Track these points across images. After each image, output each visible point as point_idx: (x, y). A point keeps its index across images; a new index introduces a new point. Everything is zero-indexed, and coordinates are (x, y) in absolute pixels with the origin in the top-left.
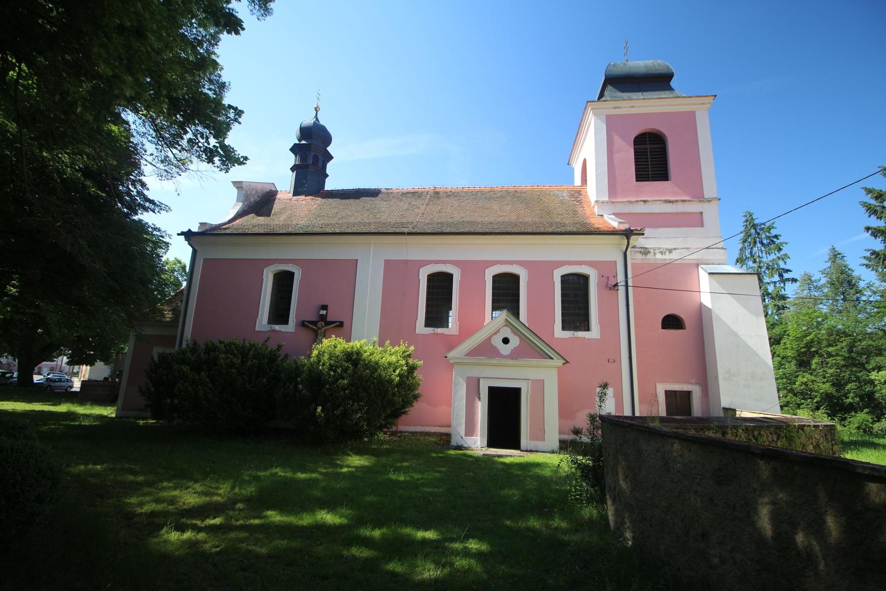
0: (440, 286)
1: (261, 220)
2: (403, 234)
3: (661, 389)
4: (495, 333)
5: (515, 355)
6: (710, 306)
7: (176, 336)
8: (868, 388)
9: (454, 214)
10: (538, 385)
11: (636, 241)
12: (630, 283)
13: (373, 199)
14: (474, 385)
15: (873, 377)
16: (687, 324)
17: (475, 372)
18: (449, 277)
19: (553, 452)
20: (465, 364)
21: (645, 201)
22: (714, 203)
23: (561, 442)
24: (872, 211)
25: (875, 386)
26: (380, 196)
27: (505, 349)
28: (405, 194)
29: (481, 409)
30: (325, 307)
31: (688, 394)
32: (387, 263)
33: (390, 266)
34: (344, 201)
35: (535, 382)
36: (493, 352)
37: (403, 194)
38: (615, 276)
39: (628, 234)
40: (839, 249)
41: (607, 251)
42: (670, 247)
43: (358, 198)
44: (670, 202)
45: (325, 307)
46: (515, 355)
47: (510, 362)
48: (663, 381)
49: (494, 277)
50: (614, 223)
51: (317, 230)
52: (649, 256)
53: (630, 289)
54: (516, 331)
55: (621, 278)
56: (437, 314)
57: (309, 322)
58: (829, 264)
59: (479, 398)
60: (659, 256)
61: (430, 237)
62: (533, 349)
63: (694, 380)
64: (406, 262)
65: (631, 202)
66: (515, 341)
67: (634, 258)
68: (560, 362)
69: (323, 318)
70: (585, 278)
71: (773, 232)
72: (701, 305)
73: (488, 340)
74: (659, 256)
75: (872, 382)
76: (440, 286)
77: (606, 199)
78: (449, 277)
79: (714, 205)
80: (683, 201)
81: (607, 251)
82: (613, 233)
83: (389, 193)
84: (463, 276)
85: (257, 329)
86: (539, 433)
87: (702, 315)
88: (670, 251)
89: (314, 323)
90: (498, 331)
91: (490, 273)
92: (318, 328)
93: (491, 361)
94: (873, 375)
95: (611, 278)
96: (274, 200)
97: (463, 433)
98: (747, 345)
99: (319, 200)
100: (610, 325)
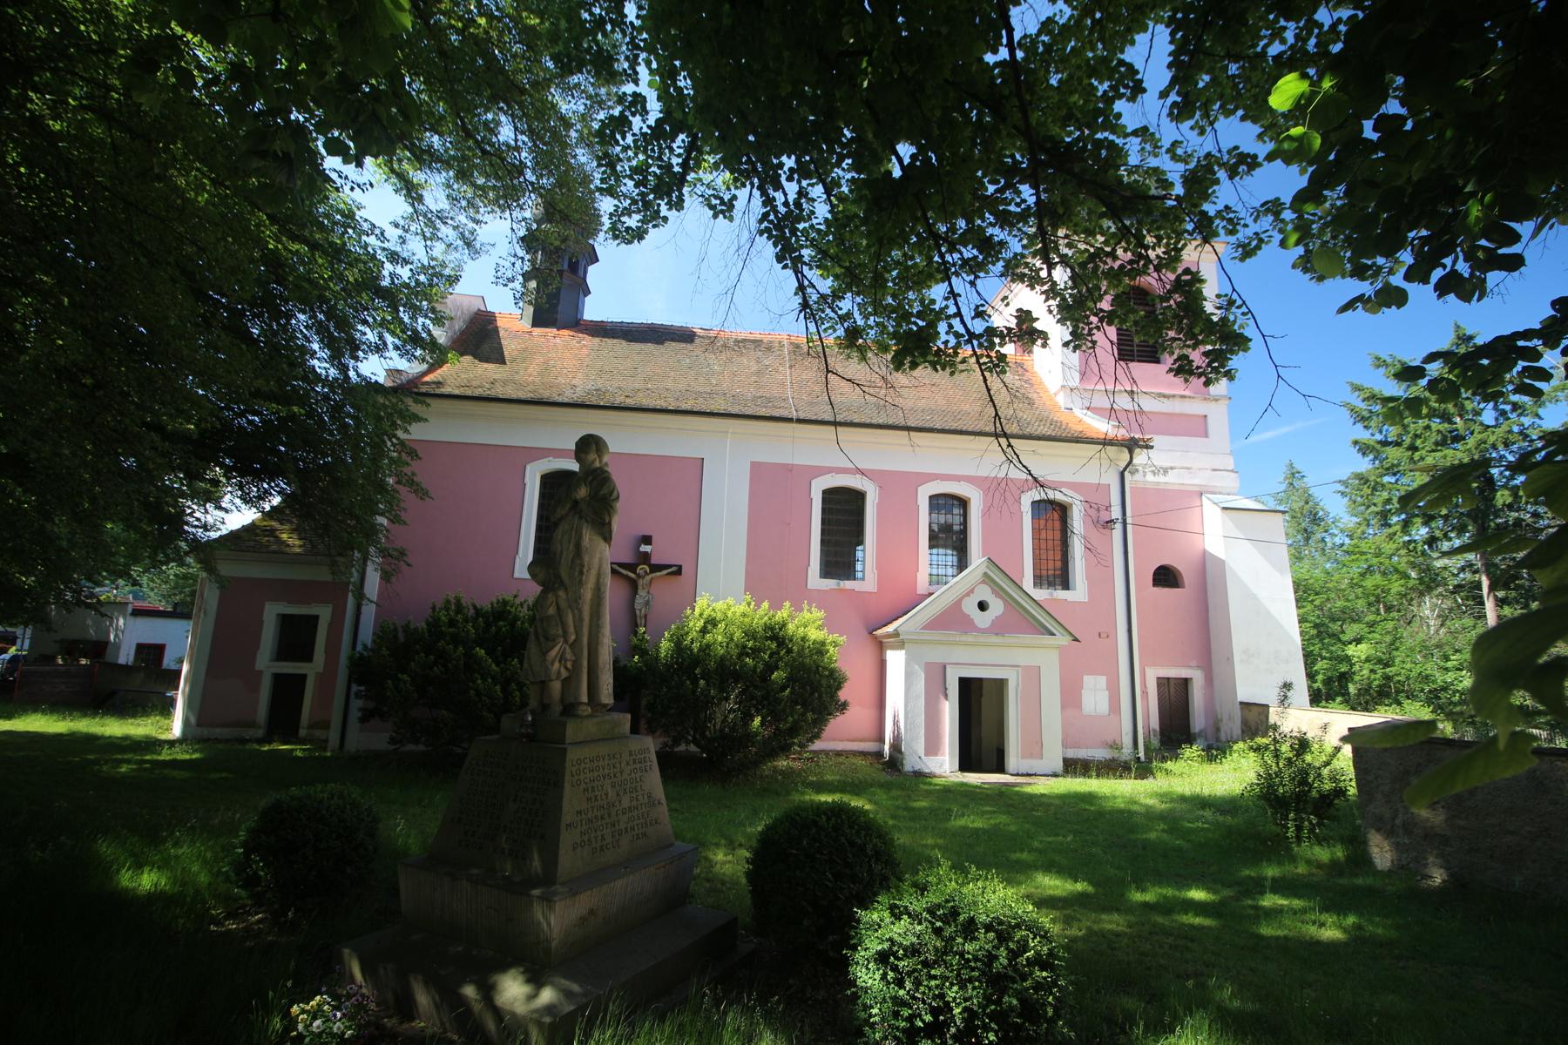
0: (844, 512)
1: (489, 370)
2: (789, 420)
3: (1152, 675)
4: (968, 595)
5: (998, 628)
6: (1222, 556)
8: (1344, 668)
10: (1033, 674)
11: (1140, 457)
12: (1129, 520)
13: (689, 346)
14: (936, 674)
15: (1350, 653)
17: (938, 655)
18: (857, 497)
19: (1055, 775)
20: (923, 642)
24: (1363, 419)
25: (1352, 665)
26: (697, 341)
27: (983, 620)
28: (741, 343)
29: (949, 712)
30: (647, 540)
31: (1185, 683)
32: (755, 466)
33: (761, 474)
35: (1027, 668)
36: (966, 625)
37: (737, 342)
39: (1131, 445)
40: (1298, 467)
41: (1095, 470)
42: (1165, 465)
44: (1165, 396)
45: (647, 540)
46: (998, 628)
47: (994, 639)
48: (1154, 665)
50: (1102, 426)
51: (619, 400)
52: (1138, 477)
53: (1129, 528)
54: (998, 591)
55: (1116, 513)
56: (839, 562)
58: (1283, 487)
59: (946, 696)
60: (1150, 478)
62: (1024, 621)
63: (1193, 663)
64: (789, 469)
66: (997, 607)
68: (1064, 640)
69: (645, 557)
71: (1364, 465)
72: (1205, 551)
73: (958, 603)
74: (1150, 478)
75: (1348, 659)
76: (844, 512)
78: (857, 497)
79: (1223, 404)
80: (1183, 397)
81: (1095, 470)
82: (1106, 442)
83: (713, 342)
86: (1035, 747)
87: (1208, 567)
88: (1166, 471)
89: (631, 567)
90: (972, 591)
91: (819, 486)
92: (639, 576)
93: (965, 638)
94: (1351, 650)
96: (496, 330)
97: (921, 752)
99: (587, 341)
100: (1101, 583)
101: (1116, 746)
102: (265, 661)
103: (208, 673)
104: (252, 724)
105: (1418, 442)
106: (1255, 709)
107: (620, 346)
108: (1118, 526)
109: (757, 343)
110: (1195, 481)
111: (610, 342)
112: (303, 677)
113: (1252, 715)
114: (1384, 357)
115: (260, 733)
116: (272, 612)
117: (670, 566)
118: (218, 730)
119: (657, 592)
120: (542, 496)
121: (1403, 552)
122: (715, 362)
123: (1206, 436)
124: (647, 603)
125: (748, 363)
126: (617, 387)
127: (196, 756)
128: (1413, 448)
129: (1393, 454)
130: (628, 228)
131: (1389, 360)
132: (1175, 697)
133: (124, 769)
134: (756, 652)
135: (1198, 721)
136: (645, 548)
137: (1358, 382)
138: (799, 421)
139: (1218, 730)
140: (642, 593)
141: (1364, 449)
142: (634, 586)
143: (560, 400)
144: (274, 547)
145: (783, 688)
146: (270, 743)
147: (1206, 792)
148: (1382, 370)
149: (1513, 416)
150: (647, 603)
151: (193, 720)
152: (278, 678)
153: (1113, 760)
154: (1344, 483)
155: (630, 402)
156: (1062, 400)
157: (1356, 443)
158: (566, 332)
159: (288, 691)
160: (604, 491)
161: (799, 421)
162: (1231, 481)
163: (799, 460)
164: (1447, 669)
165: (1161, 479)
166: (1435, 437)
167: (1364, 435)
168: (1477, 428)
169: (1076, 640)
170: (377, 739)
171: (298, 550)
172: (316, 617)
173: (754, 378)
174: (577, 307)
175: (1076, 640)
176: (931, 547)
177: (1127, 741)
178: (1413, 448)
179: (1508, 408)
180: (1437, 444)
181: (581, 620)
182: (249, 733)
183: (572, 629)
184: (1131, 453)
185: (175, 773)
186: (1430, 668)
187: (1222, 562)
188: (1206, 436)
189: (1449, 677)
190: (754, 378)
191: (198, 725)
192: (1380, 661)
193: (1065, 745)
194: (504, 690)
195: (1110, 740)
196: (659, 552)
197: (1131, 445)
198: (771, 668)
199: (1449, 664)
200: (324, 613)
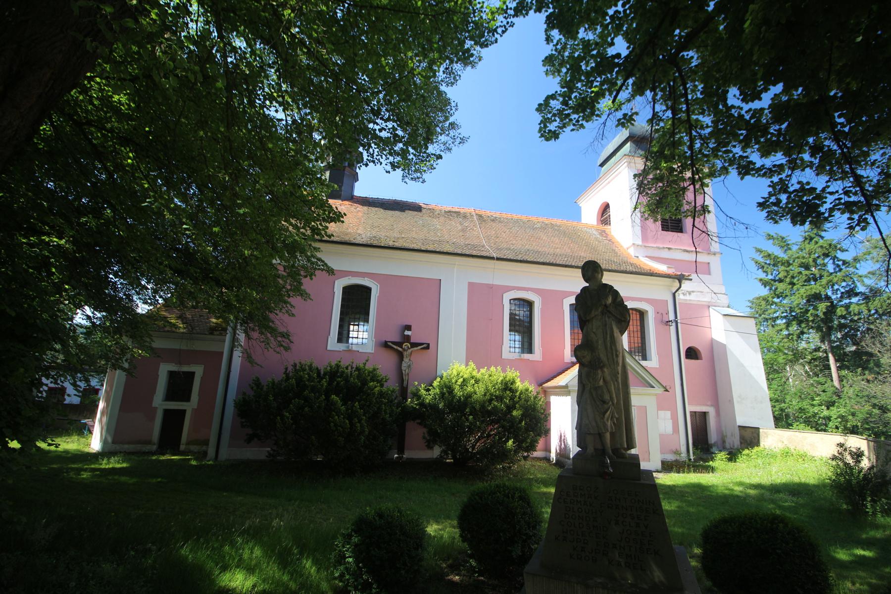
2: (493, 258)
7: (222, 353)
9: (480, 239)
16: (703, 355)
21: (669, 249)
22: (718, 256)
23: (663, 463)
26: (424, 211)
30: (409, 328)
31: (704, 415)
32: (471, 285)
34: (390, 213)
38: (667, 313)
41: (659, 291)
43: (404, 211)
44: (687, 251)
45: (409, 328)
49: (344, 288)
50: (662, 268)
55: (671, 317)
57: (393, 343)
61: (549, 267)
63: (709, 403)
64: (490, 287)
65: (659, 248)
67: (680, 297)
68: (659, 390)
70: (368, 290)
71: (764, 292)
77: (640, 243)
78: (366, 291)
79: (718, 257)
81: (659, 291)
84: (544, 304)
85: (329, 348)
87: (713, 345)
89: (400, 344)
91: (507, 297)
92: (404, 350)
95: (665, 315)
98: (750, 375)
101: (677, 452)
102: (159, 401)
103: (120, 410)
104: (149, 442)
105: (795, 281)
106: (748, 430)
107: (380, 211)
108: (674, 324)
109: (458, 213)
110: (706, 298)
111: (374, 209)
112: (184, 411)
113: (748, 434)
114: (772, 234)
115: (155, 448)
116: (164, 369)
117: (423, 344)
118: (126, 446)
119: (415, 361)
120: (343, 300)
121: (786, 340)
122: (437, 223)
123: (710, 274)
124: (409, 366)
125: (455, 224)
126: (386, 236)
127: (125, 465)
128: (793, 284)
129: (781, 287)
130: (550, 131)
131: (775, 236)
132: (700, 423)
133: (85, 475)
134: (500, 399)
135: (713, 437)
136: (407, 333)
137: (759, 247)
138: (498, 259)
139: (724, 442)
140: (406, 360)
141: (765, 283)
142: (401, 356)
143: (354, 241)
144: (167, 329)
145: (521, 421)
146: (163, 454)
147: (778, 481)
148: (771, 241)
149: (843, 267)
150: (409, 366)
151: (110, 440)
152: (167, 412)
153: (676, 461)
154: (752, 302)
155: (397, 244)
156: (632, 252)
157: (761, 280)
158: (347, 202)
159: (173, 420)
160: (619, 300)
161: (498, 259)
162: (724, 300)
163: (498, 282)
164: (813, 405)
165: (688, 297)
166: (804, 278)
167: (762, 275)
168: (825, 274)
169: (667, 390)
170: (257, 452)
171: (182, 330)
172: (193, 374)
173: (461, 234)
174: (352, 188)
175: (667, 390)
176: (510, 331)
177: (683, 449)
178: (793, 284)
179: (840, 263)
180: (805, 281)
181: (619, 390)
182: (147, 448)
183: (614, 396)
184: (680, 283)
185: (123, 479)
186: (805, 404)
187: (724, 346)
188: (710, 274)
189: (816, 409)
190: (461, 234)
191: (114, 442)
192: (777, 401)
193: (662, 453)
194: (351, 423)
195: (674, 449)
196: (415, 335)
197: (680, 278)
198: (510, 408)
199: (815, 402)
200: (198, 371)
